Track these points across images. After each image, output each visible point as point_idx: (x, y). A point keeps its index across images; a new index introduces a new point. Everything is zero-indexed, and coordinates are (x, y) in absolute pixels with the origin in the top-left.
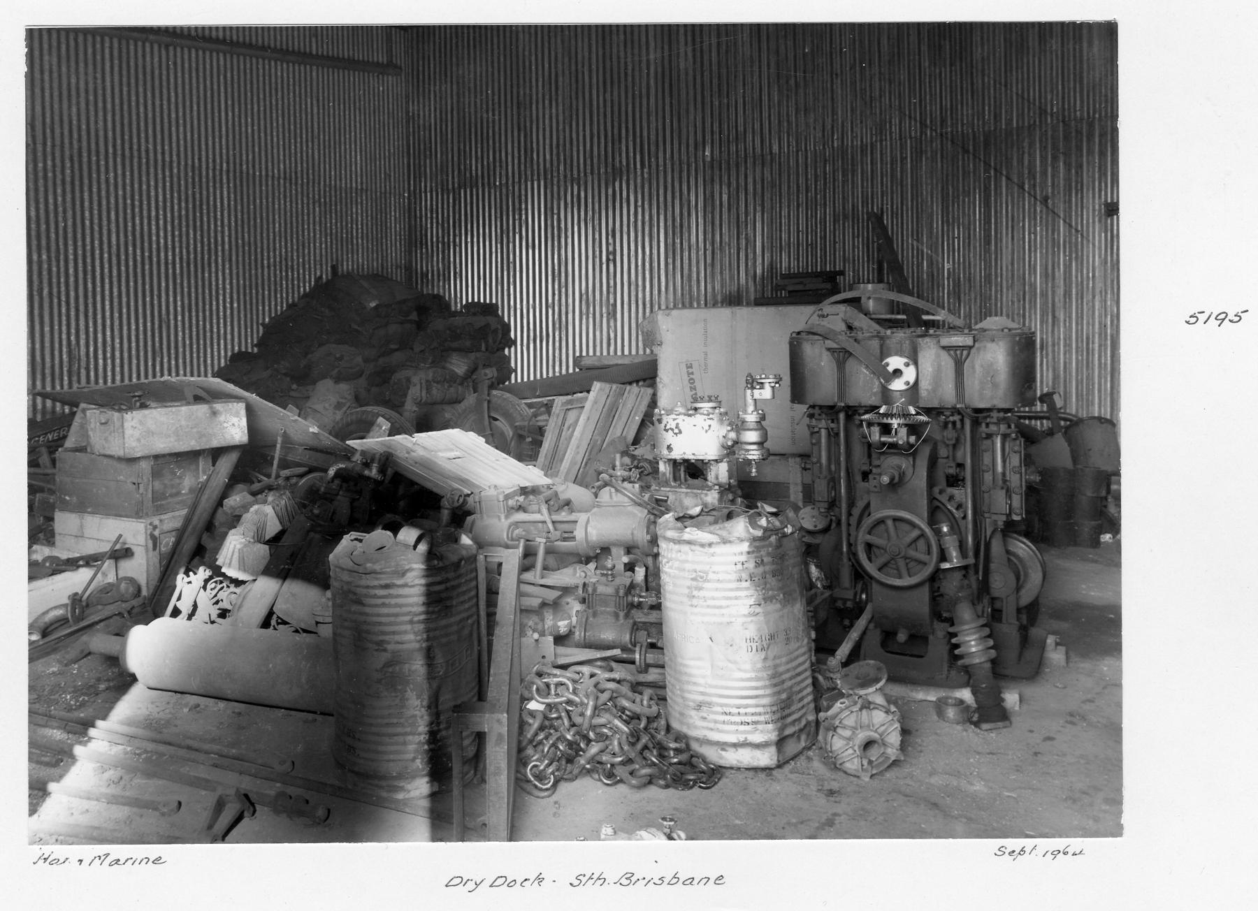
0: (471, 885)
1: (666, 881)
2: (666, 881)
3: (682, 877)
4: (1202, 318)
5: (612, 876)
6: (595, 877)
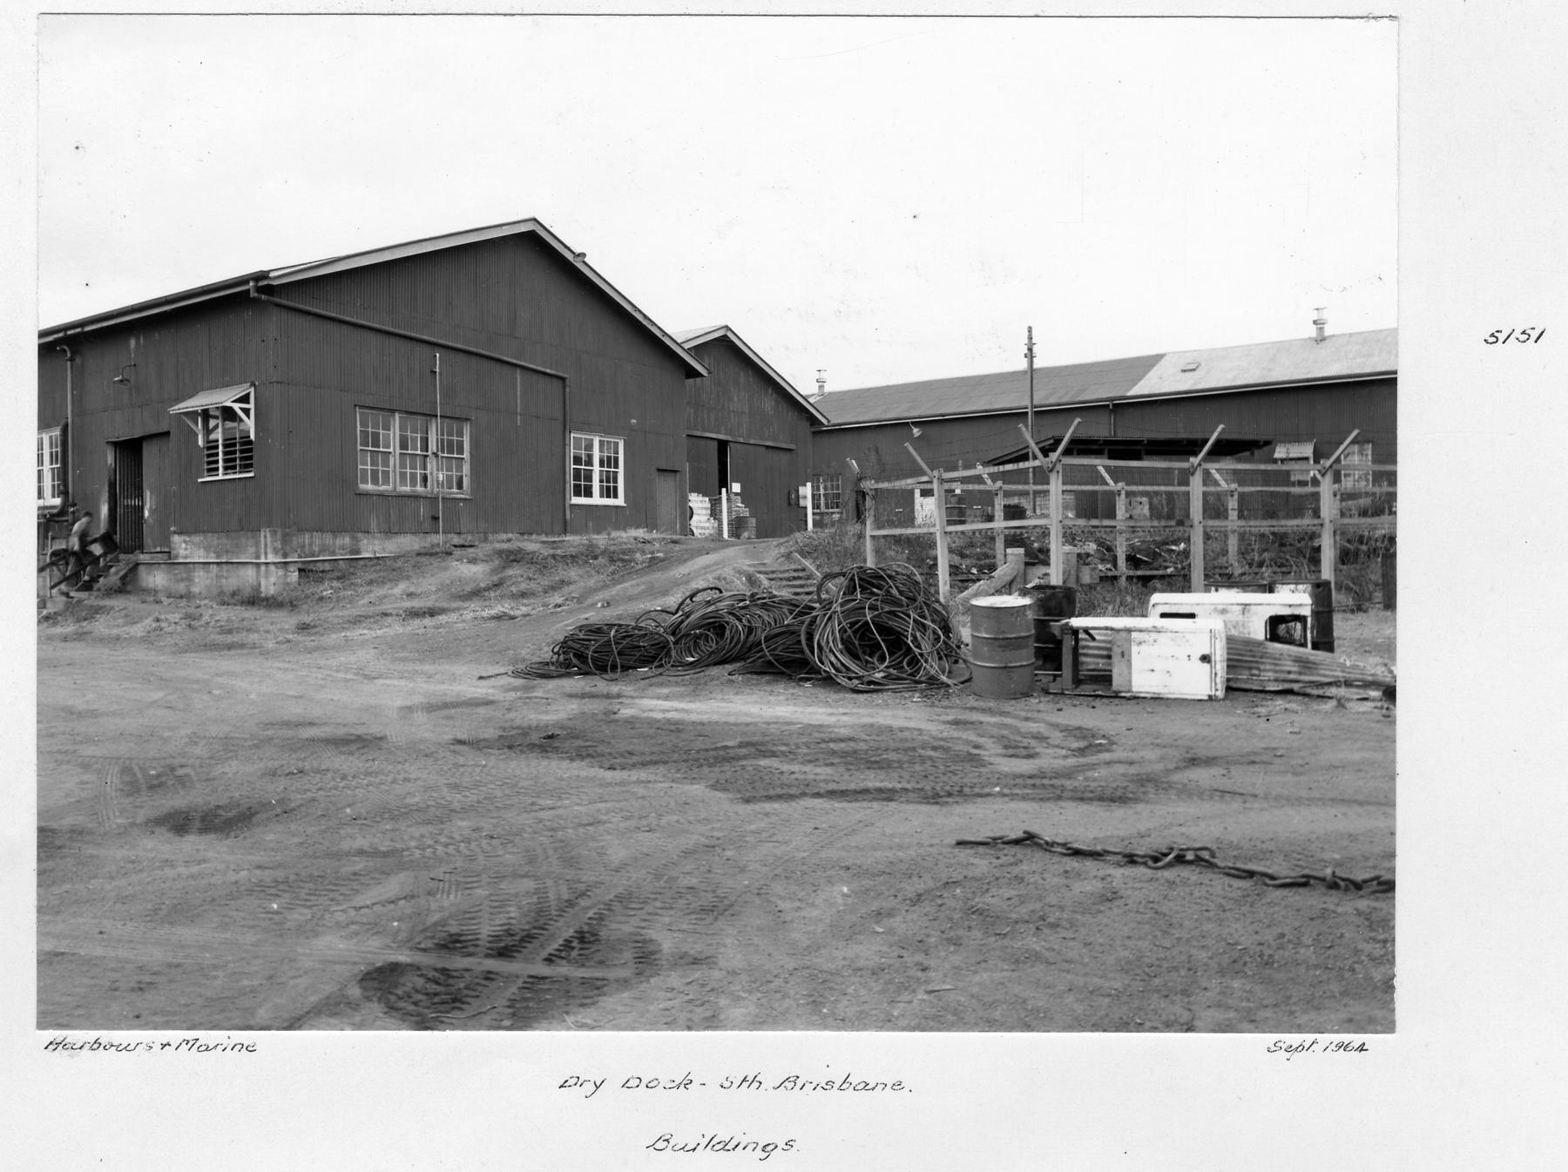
1: (836, 1086)
4: (1502, 337)
5: (770, 1080)
6: (750, 1079)
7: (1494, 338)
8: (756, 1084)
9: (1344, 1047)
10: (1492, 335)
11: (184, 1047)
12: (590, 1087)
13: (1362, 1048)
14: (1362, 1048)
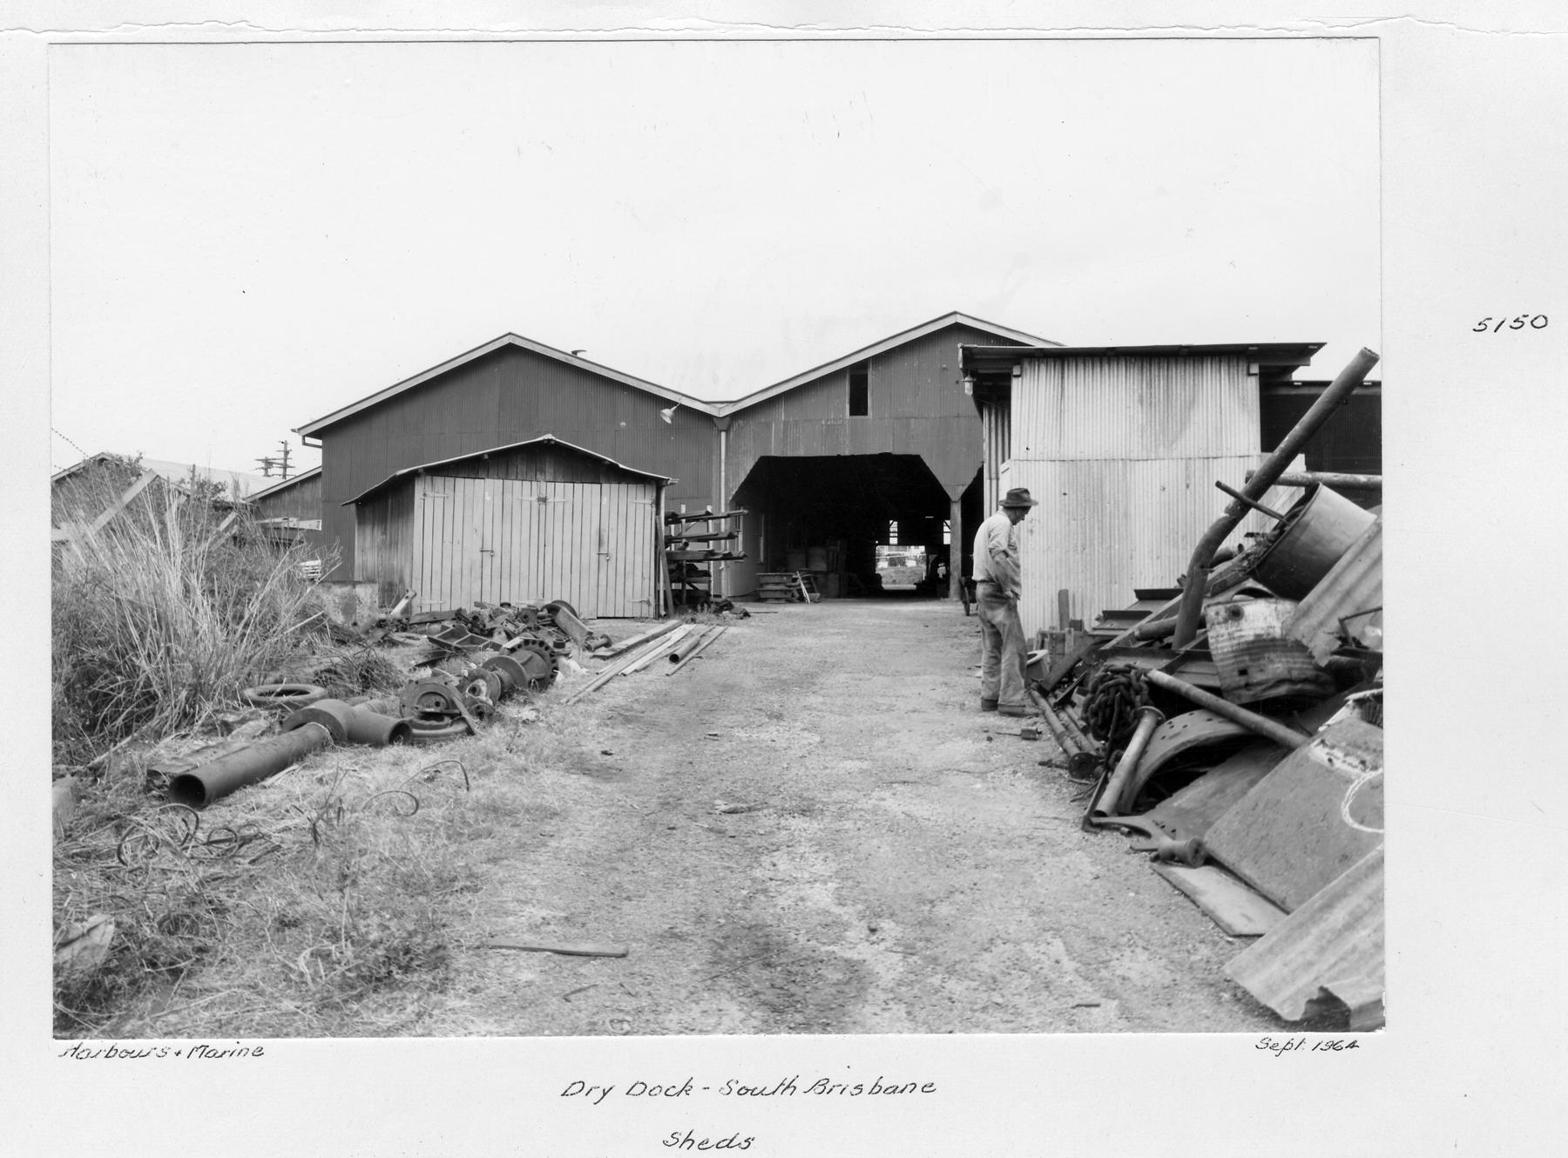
3: (884, 1084)
4: (1492, 325)
6: (787, 1083)
7: (1481, 328)
8: (791, 1089)
9: (1334, 1046)
11: (196, 1054)
12: (597, 1094)
13: (1353, 1045)
14: (1353, 1045)
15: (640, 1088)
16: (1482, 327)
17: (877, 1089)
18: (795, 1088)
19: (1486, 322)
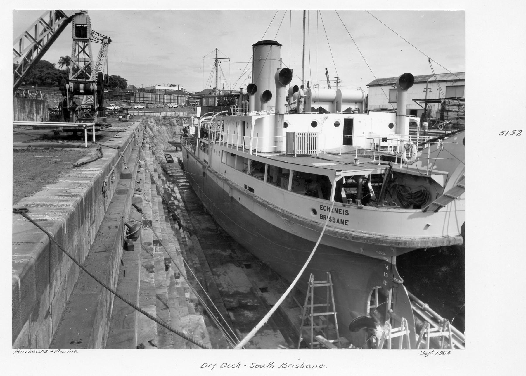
0: (211, 367)
2: (299, 366)
3: (305, 365)
4: (505, 133)
5: (277, 364)
6: (271, 364)
9: (444, 353)
10: (297, 366)
12: (211, 367)
13: (449, 353)
15: (308, 366)
16: (502, 134)
17: (302, 366)
18: (240, 364)
19: (515, 132)
